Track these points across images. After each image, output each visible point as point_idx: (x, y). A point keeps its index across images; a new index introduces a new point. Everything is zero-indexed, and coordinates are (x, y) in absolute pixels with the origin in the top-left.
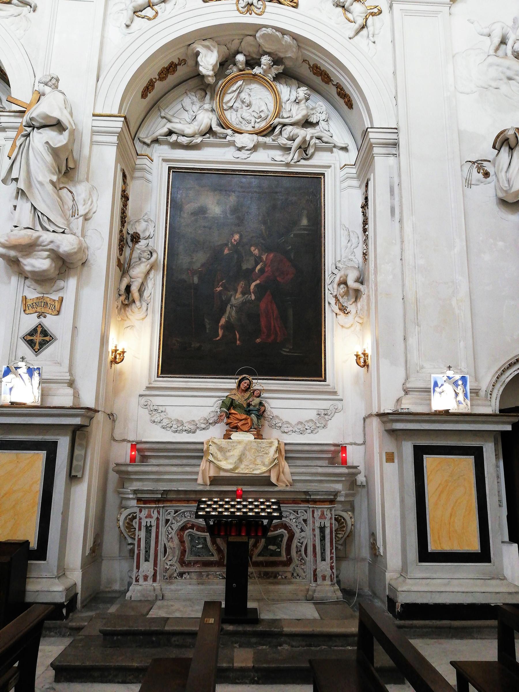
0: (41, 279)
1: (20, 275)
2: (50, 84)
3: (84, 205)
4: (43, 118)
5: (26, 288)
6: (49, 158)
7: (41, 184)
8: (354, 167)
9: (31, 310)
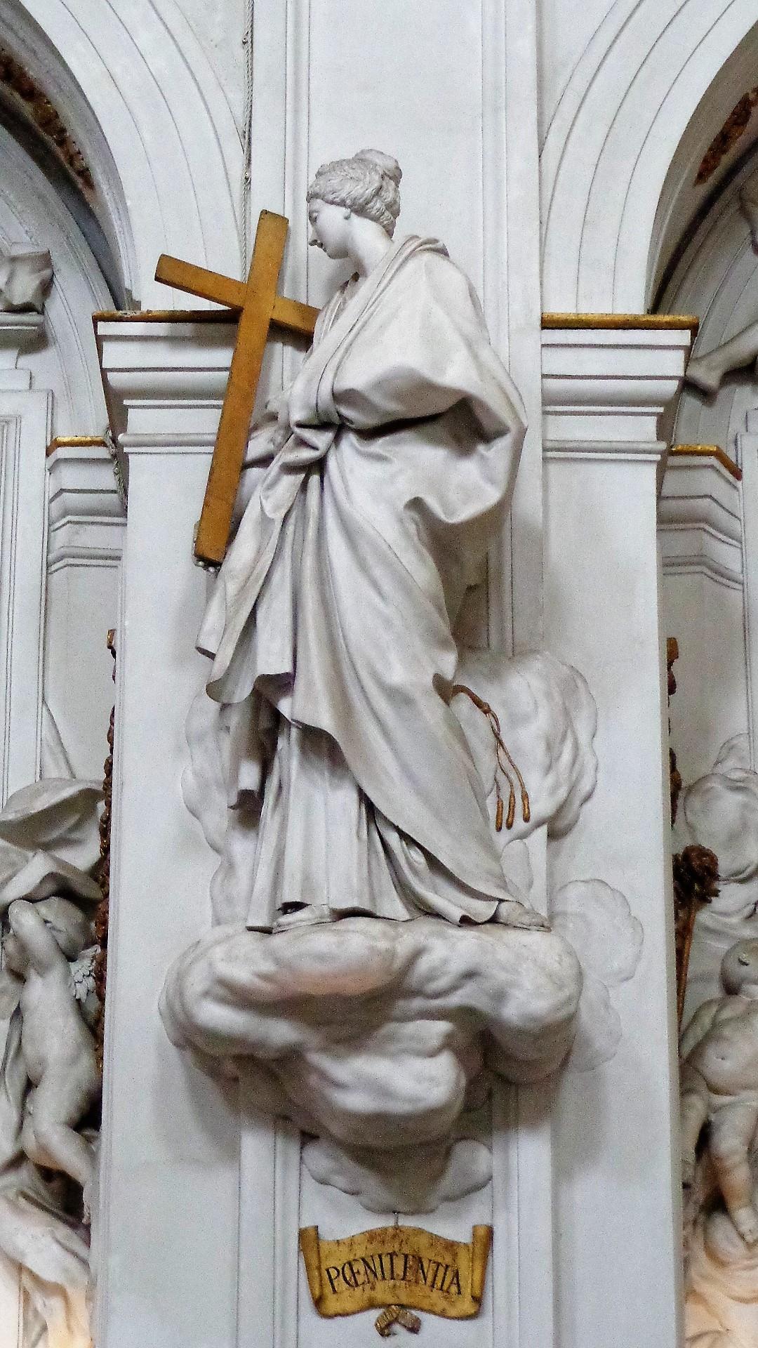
0: (402, 1155)
1: (280, 1122)
2: (377, 205)
3: (549, 769)
4: (398, 396)
5: (310, 1185)
6: (422, 571)
7: (398, 697)
9: (345, 1298)
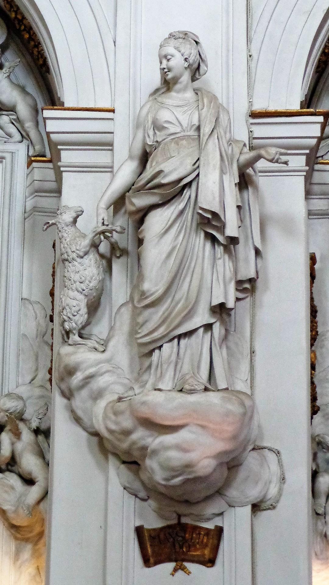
8: (50, 165)
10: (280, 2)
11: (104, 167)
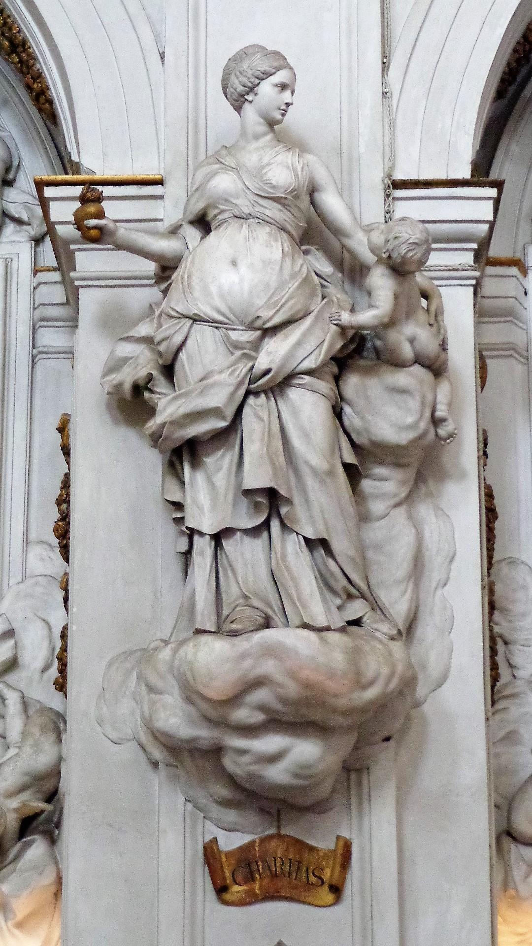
10: (435, 3)
11: (135, 278)
